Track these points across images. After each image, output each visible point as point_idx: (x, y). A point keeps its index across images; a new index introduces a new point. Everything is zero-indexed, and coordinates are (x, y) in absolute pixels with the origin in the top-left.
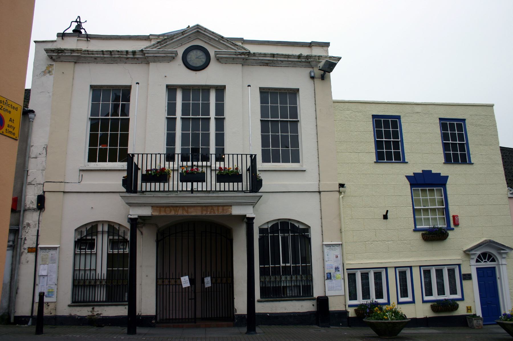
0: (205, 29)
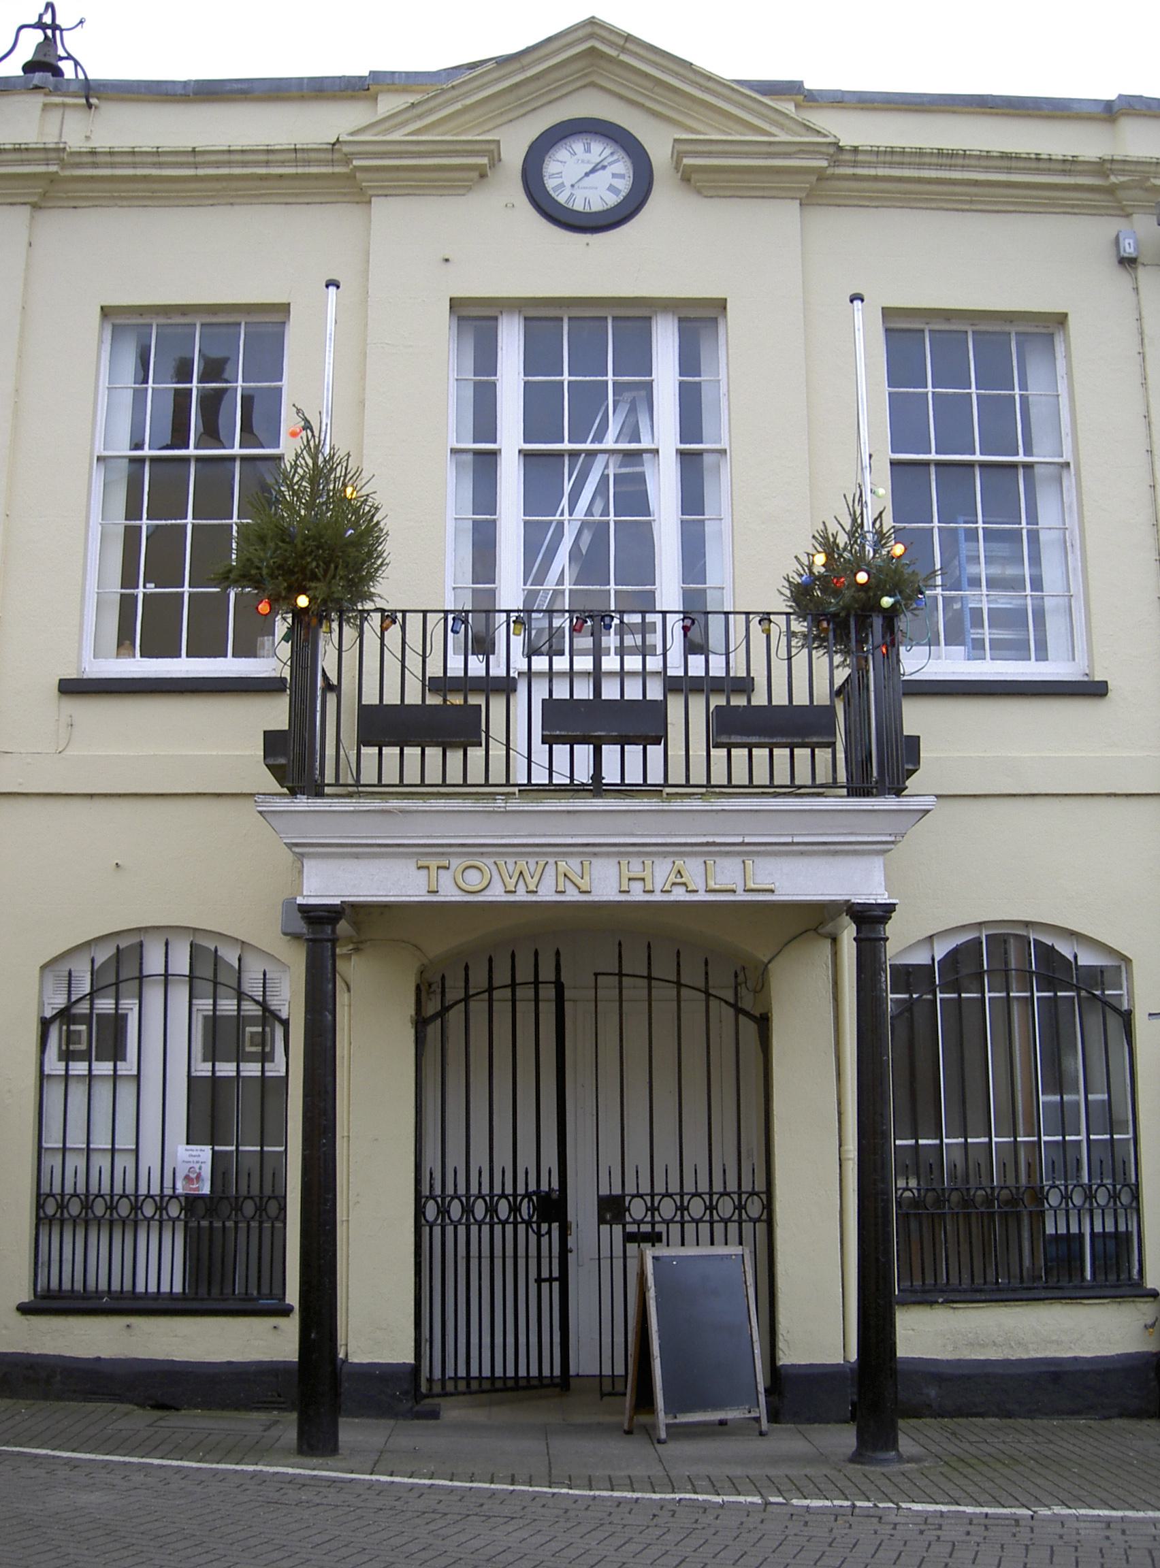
0: (629, 38)
